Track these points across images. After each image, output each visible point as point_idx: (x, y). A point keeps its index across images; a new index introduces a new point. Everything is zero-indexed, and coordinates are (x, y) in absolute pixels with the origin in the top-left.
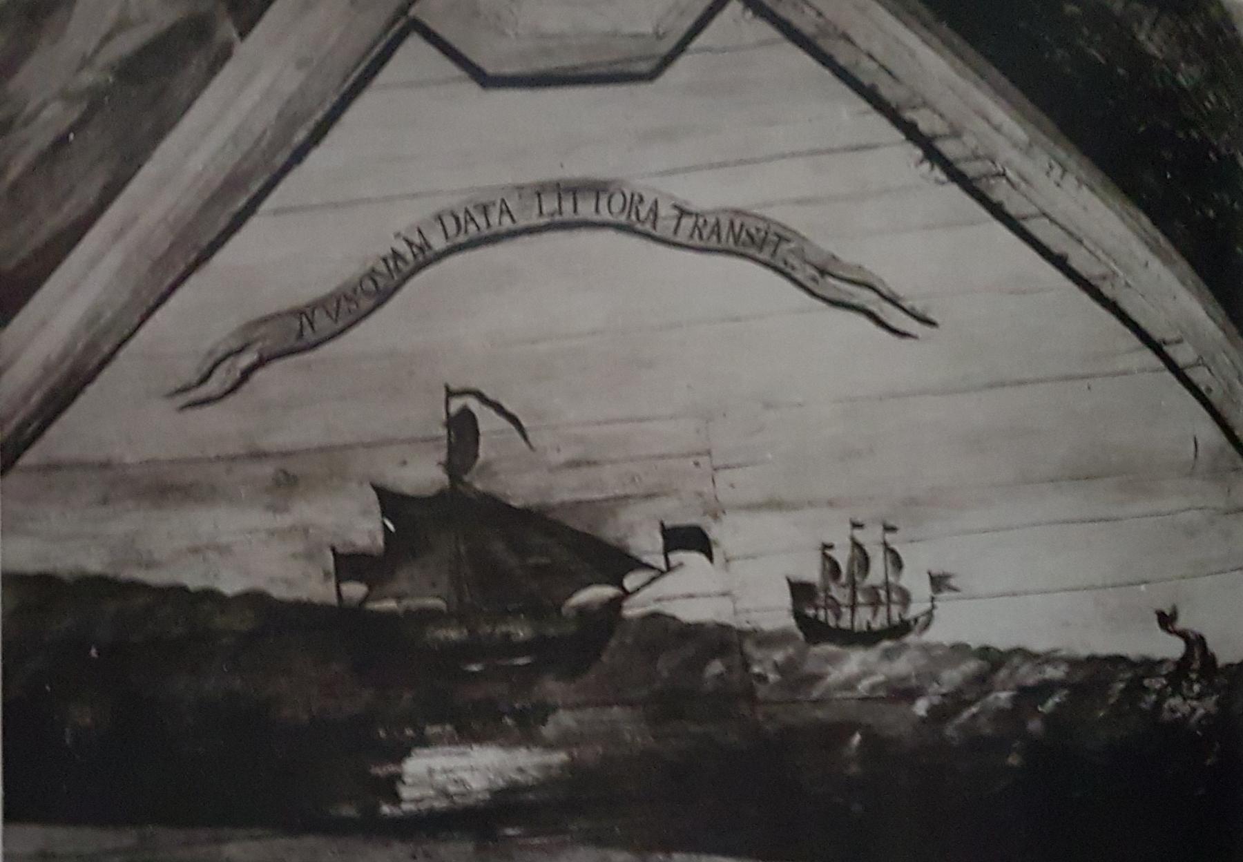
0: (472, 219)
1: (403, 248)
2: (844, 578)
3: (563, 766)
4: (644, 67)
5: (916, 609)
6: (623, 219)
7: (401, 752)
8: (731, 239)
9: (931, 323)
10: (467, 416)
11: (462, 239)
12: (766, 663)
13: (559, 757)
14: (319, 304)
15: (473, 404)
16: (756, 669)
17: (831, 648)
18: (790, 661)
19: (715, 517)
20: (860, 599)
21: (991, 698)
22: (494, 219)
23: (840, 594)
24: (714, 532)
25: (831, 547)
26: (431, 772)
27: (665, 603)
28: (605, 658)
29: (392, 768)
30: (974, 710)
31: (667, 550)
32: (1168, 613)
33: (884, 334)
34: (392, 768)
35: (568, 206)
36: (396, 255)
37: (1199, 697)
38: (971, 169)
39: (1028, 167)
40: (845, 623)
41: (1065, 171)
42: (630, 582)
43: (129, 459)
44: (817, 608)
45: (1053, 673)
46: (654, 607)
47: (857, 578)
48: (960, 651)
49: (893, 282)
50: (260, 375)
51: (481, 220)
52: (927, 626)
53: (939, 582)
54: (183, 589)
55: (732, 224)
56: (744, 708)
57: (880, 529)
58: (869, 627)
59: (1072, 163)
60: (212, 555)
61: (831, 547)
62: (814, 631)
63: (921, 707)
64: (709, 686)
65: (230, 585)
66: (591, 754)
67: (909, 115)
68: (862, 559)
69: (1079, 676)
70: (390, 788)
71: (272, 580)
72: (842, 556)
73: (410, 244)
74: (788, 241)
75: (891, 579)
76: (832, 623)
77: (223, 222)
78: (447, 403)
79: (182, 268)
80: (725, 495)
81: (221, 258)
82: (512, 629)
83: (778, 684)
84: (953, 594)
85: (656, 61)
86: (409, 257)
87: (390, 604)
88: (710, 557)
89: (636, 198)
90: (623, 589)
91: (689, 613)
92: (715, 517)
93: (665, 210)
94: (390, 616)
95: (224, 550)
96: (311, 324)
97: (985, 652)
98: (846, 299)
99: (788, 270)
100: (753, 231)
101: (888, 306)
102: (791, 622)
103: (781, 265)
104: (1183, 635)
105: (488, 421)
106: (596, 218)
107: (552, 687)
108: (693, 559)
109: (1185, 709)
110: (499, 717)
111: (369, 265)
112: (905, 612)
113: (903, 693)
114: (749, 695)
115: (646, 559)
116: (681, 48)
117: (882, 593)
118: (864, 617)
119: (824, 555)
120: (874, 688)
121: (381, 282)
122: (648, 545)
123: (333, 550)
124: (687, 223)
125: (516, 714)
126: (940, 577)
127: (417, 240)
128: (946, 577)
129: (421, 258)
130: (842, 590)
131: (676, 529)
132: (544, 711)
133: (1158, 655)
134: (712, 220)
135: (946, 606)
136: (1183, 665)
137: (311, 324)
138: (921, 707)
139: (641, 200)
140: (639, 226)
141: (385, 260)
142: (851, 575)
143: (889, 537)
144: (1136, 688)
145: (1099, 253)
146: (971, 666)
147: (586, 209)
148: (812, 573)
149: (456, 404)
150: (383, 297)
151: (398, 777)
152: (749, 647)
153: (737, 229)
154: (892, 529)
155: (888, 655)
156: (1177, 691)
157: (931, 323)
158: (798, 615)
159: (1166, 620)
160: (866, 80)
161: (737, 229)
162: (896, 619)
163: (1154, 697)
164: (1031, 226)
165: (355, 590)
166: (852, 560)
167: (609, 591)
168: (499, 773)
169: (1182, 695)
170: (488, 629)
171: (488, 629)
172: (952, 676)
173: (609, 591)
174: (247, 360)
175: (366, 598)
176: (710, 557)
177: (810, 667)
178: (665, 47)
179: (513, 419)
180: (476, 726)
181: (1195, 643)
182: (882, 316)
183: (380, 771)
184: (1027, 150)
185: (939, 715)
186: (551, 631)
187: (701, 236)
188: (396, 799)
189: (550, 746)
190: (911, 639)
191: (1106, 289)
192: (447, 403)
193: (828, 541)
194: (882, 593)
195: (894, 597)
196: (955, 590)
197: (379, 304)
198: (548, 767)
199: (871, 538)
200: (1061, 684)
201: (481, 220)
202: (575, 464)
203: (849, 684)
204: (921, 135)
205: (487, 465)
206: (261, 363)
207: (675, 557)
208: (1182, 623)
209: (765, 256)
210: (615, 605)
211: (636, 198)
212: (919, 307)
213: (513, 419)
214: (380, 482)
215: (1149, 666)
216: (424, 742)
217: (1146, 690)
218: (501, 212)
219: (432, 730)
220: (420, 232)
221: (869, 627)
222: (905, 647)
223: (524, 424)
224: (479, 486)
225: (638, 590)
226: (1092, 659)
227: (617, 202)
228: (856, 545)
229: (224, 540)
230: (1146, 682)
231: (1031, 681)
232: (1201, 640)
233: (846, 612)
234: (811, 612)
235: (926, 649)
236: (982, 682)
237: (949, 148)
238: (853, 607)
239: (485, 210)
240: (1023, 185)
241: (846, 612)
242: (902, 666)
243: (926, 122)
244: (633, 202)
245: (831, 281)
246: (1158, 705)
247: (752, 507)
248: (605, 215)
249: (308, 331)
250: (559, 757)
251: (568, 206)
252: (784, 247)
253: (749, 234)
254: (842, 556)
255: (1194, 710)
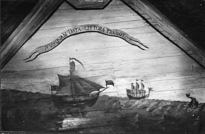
0: (74, 31)
1: (62, 35)
2: (135, 89)
3: (89, 121)
4: (102, 7)
5: (147, 94)
6: (98, 31)
7: (62, 119)
8: (116, 34)
9: (148, 48)
10: (73, 63)
11: (72, 34)
12: (123, 103)
13: (89, 119)
14: (49, 44)
15: (74, 60)
16: (121, 104)
17: (133, 100)
18: (127, 103)
19: (114, 79)
20: (138, 92)
21: (158, 108)
22: (78, 30)
23: (135, 92)
24: (114, 82)
25: (133, 84)
26: (67, 122)
27: (106, 93)
28: (96, 103)
29: (61, 122)
30: (156, 110)
31: (106, 85)
32: (188, 94)
33: (140, 49)
34: (61, 122)
35: (90, 28)
36: (61, 36)
37: (195, 108)
38: (153, 24)
39: (162, 23)
40: (135, 96)
41: (168, 24)
42: (101, 90)
43: (18, 71)
44: (131, 94)
45: (168, 104)
46: (104, 94)
47: (137, 89)
48: (154, 100)
49: (142, 41)
50: (39, 56)
51: (75, 31)
52: (148, 97)
53: (150, 89)
54: (26, 92)
55: (116, 32)
56: (119, 110)
57: (140, 81)
58: (139, 97)
59: (169, 23)
60: (31, 87)
61: (133, 84)
62: (130, 97)
63: (148, 109)
64: (113, 107)
65: (34, 91)
66: (94, 119)
67: (143, 16)
68: (138, 86)
69: (173, 104)
70: (60, 125)
71: (41, 91)
72: (135, 85)
73: (64, 34)
74: (125, 35)
75: (142, 89)
76: (133, 96)
77: (33, 31)
78: (70, 61)
79: (27, 39)
80: (115, 75)
81: (33, 37)
82: (80, 98)
83: (125, 107)
84: (153, 91)
85: (103, 6)
86: (64, 37)
87: (60, 94)
88: (114, 86)
89: (101, 27)
90: (99, 91)
91: (111, 95)
92: (114, 79)
93: (105, 30)
94: (61, 97)
95: (33, 85)
96: (47, 48)
97: (157, 100)
98: (135, 44)
99: (125, 39)
100: (119, 33)
101: (141, 45)
102: (127, 96)
103: (124, 38)
104: (191, 98)
105: (76, 63)
106: (94, 30)
107: (87, 108)
108: (111, 86)
109: (191, 110)
110: (78, 113)
111: (57, 38)
112: (145, 94)
113: (145, 107)
114: (120, 108)
115: (103, 86)
116: (107, 5)
117: (141, 91)
118: (139, 95)
119: (132, 85)
120: (140, 107)
121: (59, 41)
122: (103, 84)
123: (51, 85)
124: (109, 31)
125: (81, 112)
126: (150, 88)
127: (65, 34)
128: (151, 88)
129: (66, 37)
130: (135, 91)
131: (127, 90)
132: (86, 112)
133: (186, 101)
134: (113, 31)
135: (151, 93)
136: (191, 103)
137: (47, 48)
138: (148, 109)
139: (102, 28)
140: (101, 32)
141: (60, 37)
142: (136, 88)
143: (142, 82)
144: (182, 106)
145: (174, 37)
146: (155, 103)
147: (93, 29)
148: (130, 88)
149: (71, 61)
150: (59, 43)
151: (62, 123)
152: (120, 100)
153: (117, 33)
154: (143, 81)
155: (142, 101)
156: (190, 107)
157: (148, 48)
158: (128, 95)
159: (188, 96)
160: (136, 10)
161: (117, 33)
162: (143, 96)
163: (186, 108)
164: (162, 32)
165: (55, 92)
166: (136, 85)
167: (97, 92)
168: (79, 122)
169: (191, 108)
170: (77, 98)
171: (77, 98)
172: (152, 104)
173: (97, 92)
174: (37, 54)
175: (56, 93)
176: (114, 86)
177: (130, 104)
178: (105, 4)
179: (81, 63)
180: (75, 115)
181: (193, 99)
182: (140, 47)
183: (59, 122)
184: (162, 21)
185: (151, 111)
186: (87, 98)
187: (111, 34)
188: (61, 127)
189: (87, 118)
190: (146, 98)
191: (175, 42)
192: (70, 61)
193: (133, 83)
194: (141, 91)
195: (143, 92)
196: (153, 90)
197: (59, 44)
198: (87, 121)
199: (139, 82)
200: (170, 106)
201: (75, 31)
202: (91, 70)
203: (137, 106)
204: (145, 19)
205: (77, 71)
206: (39, 54)
207: (108, 86)
208: (191, 96)
209: (121, 37)
210: (98, 94)
211: (101, 27)
212: (146, 45)
213: (81, 63)
214: (59, 74)
215: (185, 103)
216: (66, 117)
217: (184, 107)
218: (79, 30)
219: (67, 115)
220: (65, 33)
221: (139, 97)
222: (145, 100)
223: (83, 64)
224: (75, 74)
225: (102, 91)
226: (175, 101)
227: (98, 28)
228: (137, 83)
229: (33, 84)
230: (184, 105)
231: (165, 105)
232: (195, 99)
233: (136, 94)
234: (130, 94)
235: (148, 100)
236: (157, 105)
237: (150, 21)
238: (137, 93)
239: (76, 29)
240: (161, 27)
241: (136, 94)
242: (144, 103)
243: (146, 17)
244: (100, 28)
245: (132, 41)
246: (186, 110)
247: (121, 77)
248: (96, 30)
249: (47, 49)
250: (89, 119)
251: (90, 28)
252: (124, 35)
253: (119, 33)
254: (135, 85)
255: (193, 111)
